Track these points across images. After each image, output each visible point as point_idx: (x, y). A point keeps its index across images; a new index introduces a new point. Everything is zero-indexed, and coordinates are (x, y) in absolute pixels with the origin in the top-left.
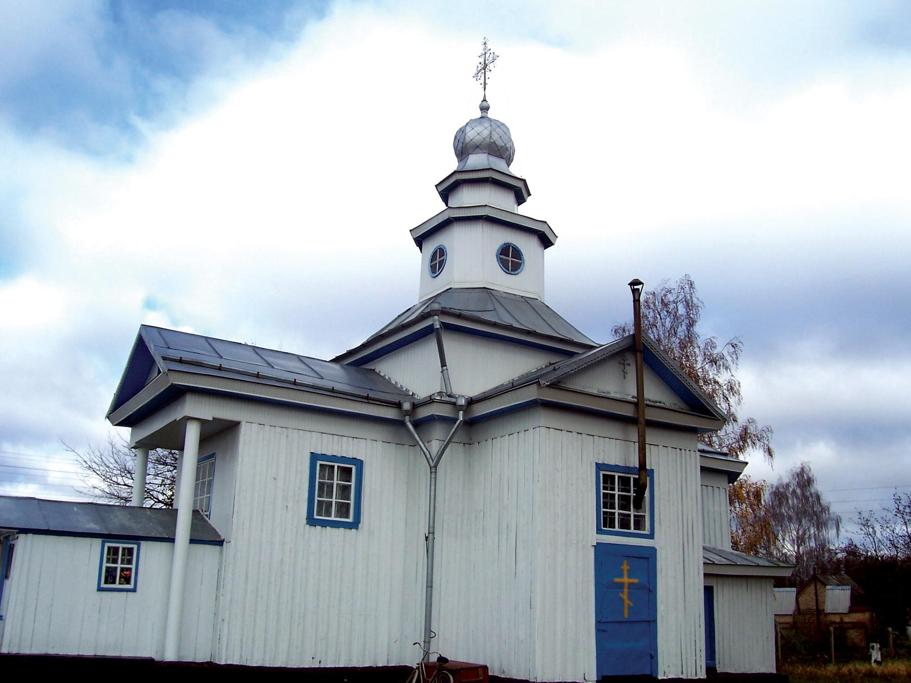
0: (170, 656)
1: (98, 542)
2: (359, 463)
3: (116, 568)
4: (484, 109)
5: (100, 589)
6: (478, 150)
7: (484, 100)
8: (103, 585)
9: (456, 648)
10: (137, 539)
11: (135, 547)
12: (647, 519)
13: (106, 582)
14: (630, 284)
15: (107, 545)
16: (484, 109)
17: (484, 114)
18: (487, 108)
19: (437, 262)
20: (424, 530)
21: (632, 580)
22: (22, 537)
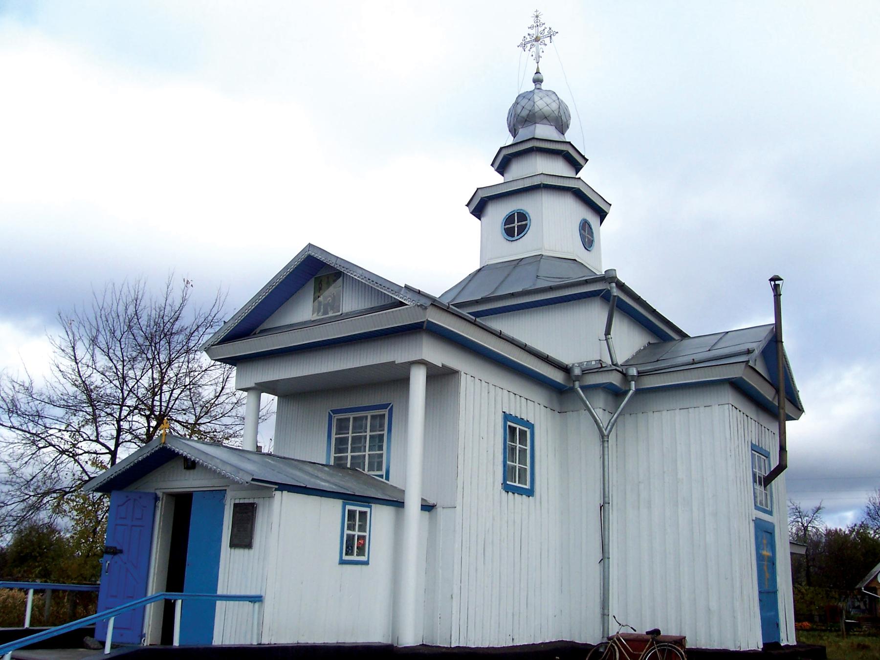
0: (409, 639)
1: (338, 503)
2: (528, 424)
3: (354, 536)
4: (538, 81)
5: (342, 562)
6: (545, 121)
7: (537, 73)
8: (345, 558)
9: (634, 617)
10: (368, 500)
11: (368, 510)
12: (528, 452)
13: (346, 554)
14: (771, 280)
15: (348, 507)
16: (538, 81)
17: (538, 86)
18: (541, 81)
19: (516, 226)
20: (598, 501)
21: (349, 458)
22: (283, 502)
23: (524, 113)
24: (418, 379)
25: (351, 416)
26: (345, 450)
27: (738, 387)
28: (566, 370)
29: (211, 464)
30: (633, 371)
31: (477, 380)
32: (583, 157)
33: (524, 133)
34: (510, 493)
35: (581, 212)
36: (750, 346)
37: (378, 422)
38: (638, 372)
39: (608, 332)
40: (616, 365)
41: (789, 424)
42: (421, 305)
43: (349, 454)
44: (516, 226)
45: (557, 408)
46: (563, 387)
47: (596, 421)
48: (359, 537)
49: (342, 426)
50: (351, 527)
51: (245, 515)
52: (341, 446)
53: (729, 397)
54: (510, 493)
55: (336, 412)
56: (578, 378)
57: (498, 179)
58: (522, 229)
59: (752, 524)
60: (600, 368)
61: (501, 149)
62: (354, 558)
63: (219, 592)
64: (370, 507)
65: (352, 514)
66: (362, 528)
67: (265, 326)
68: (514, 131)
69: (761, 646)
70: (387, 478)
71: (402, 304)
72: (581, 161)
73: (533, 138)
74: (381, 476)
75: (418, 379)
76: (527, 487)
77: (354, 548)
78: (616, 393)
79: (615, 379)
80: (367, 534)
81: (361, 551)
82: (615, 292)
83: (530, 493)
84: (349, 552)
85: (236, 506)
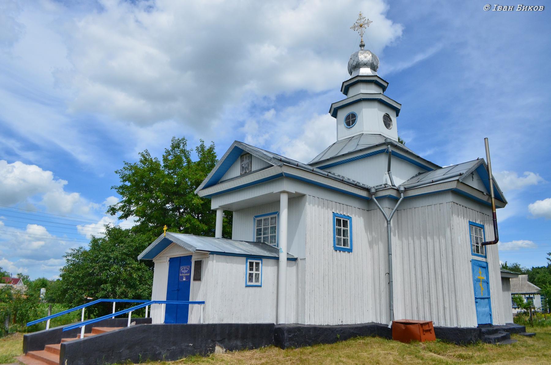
11: (260, 261)
23: (355, 64)
24: (284, 199)
25: (263, 218)
26: (260, 234)
27: (455, 192)
28: (368, 190)
29: (178, 243)
30: (402, 189)
31: (316, 198)
32: (385, 82)
33: (354, 74)
34: (338, 251)
35: (385, 111)
36: (461, 172)
37: (274, 220)
38: (405, 189)
39: (389, 170)
40: (394, 186)
41: (498, 211)
42: (279, 166)
43: (262, 236)
44: (351, 120)
45: (366, 208)
46: (368, 199)
47: (384, 214)
48: (256, 274)
49: (259, 222)
50: (251, 269)
51: (199, 264)
52: (259, 232)
53: (450, 198)
54: (338, 251)
55: (256, 217)
56: (374, 194)
57: (345, 97)
58: (354, 122)
59: (470, 264)
60: (385, 187)
61: (343, 83)
62: (254, 283)
63: (190, 300)
64: (262, 260)
65: (251, 264)
66: (257, 270)
67: (222, 180)
68: (351, 73)
69: (476, 325)
70: (278, 246)
71: (272, 166)
72: (385, 85)
73: (358, 76)
74: (275, 245)
75: (284, 199)
76: (349, 248)
77: (253, 279)
78: (394, 200)
79: (393, 193)
80: (260, 272)
81: (257, 280)
82: (391, 149)
83: (350, 251)
84: (251, 280)
85: (196, 262)
